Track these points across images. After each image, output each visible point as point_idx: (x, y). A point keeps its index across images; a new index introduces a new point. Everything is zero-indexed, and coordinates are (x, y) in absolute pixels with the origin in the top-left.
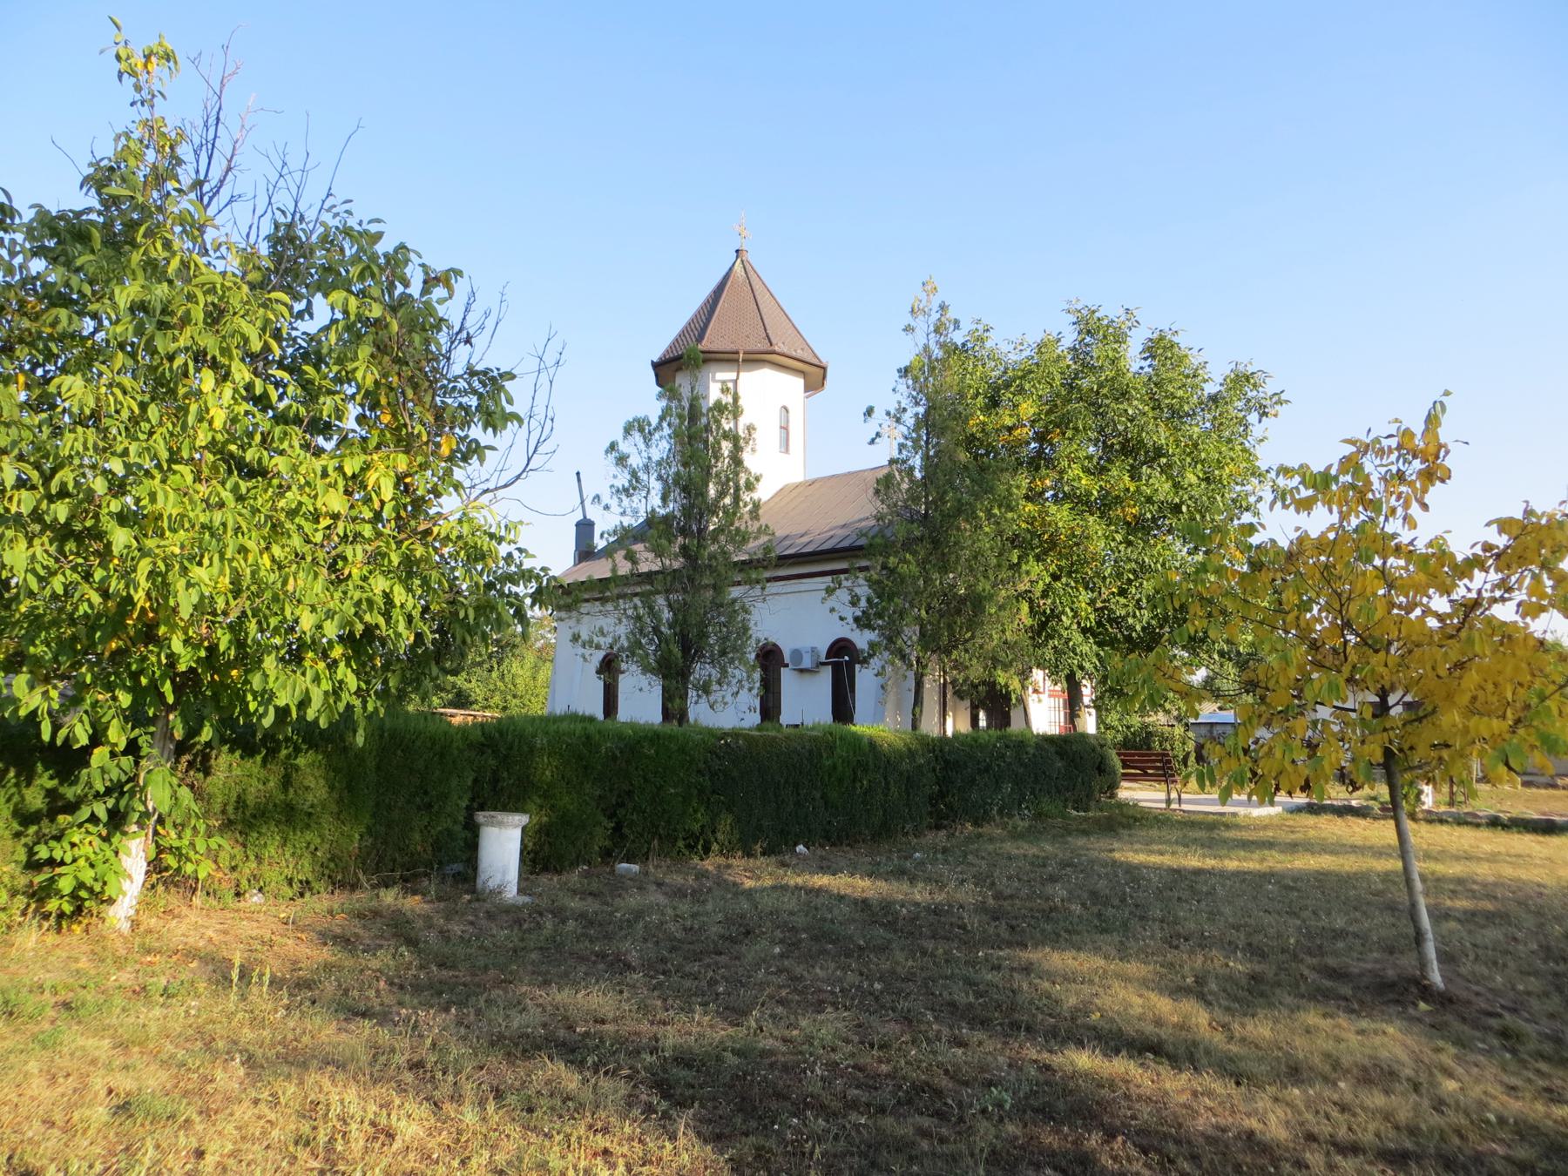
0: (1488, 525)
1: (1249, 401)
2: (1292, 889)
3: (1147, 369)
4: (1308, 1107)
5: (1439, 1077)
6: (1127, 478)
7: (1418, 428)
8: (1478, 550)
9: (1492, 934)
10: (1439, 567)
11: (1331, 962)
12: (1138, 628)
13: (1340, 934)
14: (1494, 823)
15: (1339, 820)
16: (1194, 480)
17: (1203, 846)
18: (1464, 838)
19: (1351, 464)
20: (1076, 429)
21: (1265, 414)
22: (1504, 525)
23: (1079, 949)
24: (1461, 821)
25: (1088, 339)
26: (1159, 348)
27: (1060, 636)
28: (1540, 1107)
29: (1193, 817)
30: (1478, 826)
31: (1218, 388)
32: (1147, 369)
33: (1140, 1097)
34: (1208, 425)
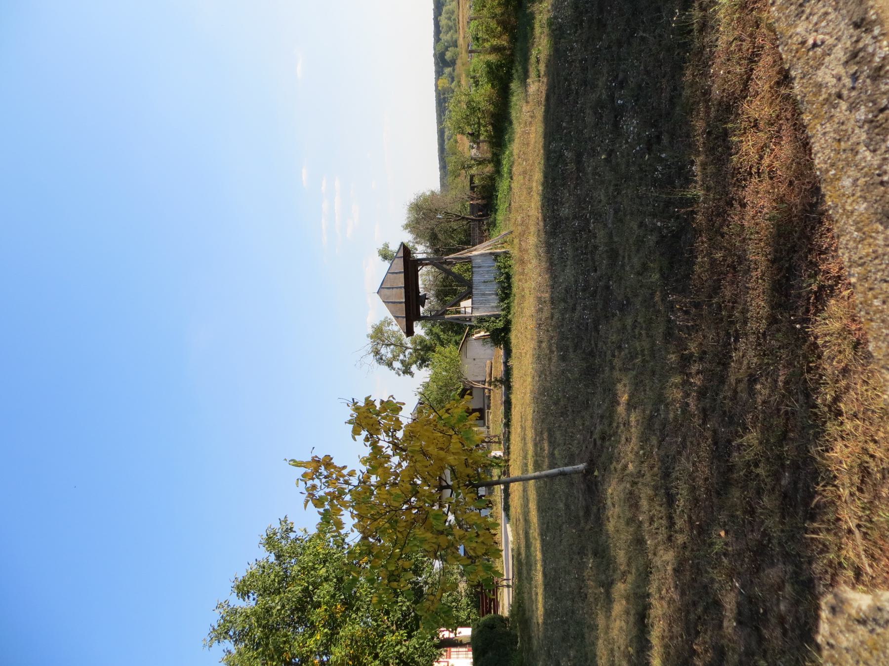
0: (355, 440)
1: (282, 538)
2: (548, 526)
3: (255, 596)
4: (656, 538)
5: (627, 472)
6: (318, 610)
7: (303, 470)
8: (368, 444)
9: (558, 434)
10: (376, 460)
11: (581, 514)
12: (408, 604)
13: (567, 506)
14: (507, 425)
15: (512, 496)
16: (324, 570)
17: (530, 570)
18: (515, 439)
19: (319, 502)
20: (285, 642)
21: (291, 528)
22: (356, 432)
23: (595, 655)
24: (508, 439)
25: (231, 633)
26: (243, 590)
27: (412, 654)
28: (633, 430)
29: (516, 572)
30: (509, 432)
31: (272, 555)
32: (255, 596)
33: (670, 631)
34: (293, 561)
